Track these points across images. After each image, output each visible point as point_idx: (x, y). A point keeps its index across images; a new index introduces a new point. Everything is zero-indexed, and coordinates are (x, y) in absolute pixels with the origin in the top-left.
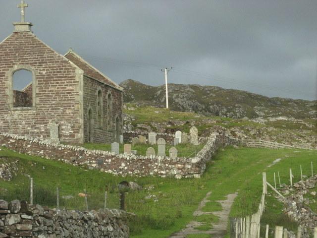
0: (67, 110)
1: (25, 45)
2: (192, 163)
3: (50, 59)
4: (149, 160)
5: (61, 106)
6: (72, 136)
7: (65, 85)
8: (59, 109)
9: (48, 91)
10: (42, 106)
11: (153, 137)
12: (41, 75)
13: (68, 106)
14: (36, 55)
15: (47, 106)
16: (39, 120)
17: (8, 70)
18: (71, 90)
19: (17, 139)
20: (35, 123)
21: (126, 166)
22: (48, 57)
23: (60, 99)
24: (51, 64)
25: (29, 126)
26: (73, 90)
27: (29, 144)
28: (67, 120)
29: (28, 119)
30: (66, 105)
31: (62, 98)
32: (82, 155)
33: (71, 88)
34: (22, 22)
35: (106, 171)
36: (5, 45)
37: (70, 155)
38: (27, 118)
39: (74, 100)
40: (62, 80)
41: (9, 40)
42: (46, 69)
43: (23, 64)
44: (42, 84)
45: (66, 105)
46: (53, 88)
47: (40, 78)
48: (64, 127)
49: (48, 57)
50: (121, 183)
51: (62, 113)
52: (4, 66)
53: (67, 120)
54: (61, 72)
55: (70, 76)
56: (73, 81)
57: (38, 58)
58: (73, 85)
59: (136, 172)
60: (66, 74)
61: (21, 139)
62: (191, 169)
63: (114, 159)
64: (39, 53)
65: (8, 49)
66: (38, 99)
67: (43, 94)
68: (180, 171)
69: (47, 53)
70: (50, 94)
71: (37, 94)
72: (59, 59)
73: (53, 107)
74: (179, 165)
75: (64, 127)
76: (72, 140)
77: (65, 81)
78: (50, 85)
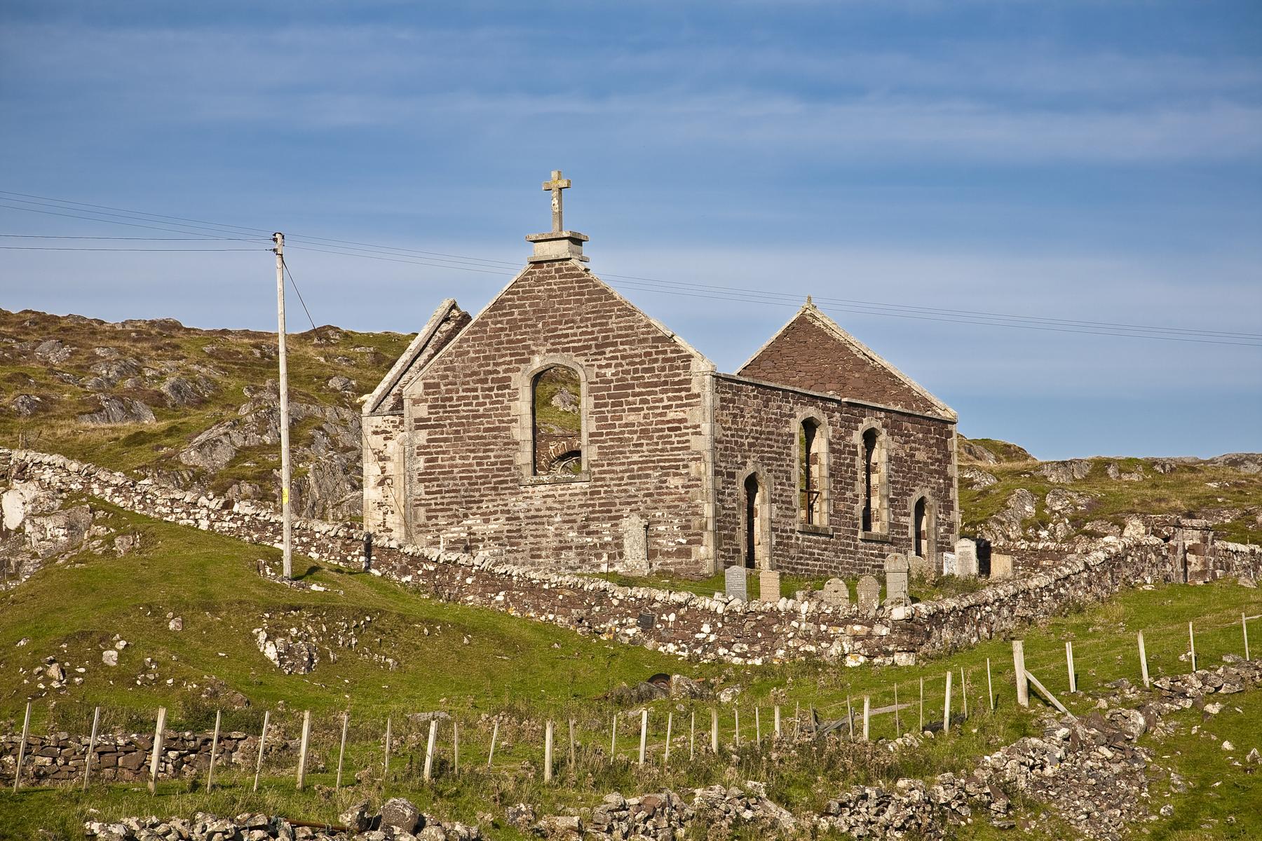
0: (669, 479)
1: (561, 296)
2: (893, 622)
3: (623, 332)
4: (774, 614)
5: (654, 468)
6: (684, 552)
7: (664, 407)
8: (648, 476)
9: (620, 426)
10: (606, 468)
11: (968, 553)
12: (601, 382)
13: (670, 467)
14: (589, 323)
15: (618, 468)
16: (597, 508)
17: (519, 370)
18: (680, 421)
19: (441, 561)
20: (586, 520)
21: (712, 632)
22: (620, 329)
23: (651, 447)
24: (626, 347)
25: (572, 528)
26: (685, 420)
27: (470, 575)
28: (669, 507)
29: (569, 508)
30: (667, 464)
31: (657, 444)
32: (601, 604)
33: (681, 415)
34: (554, 231)
35: (661, 649)
36: (509, 300)
37: (569, 603)
38: (567, 504)
39: (688, 448)
40: (656, 393)
41: (518, 287)
42: (613, 362)
43: (556, 351)
44: (605, 405)
45: (667, 464)
46: (632, 418)
47: (600, 389)
48: (661, 528)
49: (620, 329)
50: (651, 680)
51: (657, 488)
52: (508, 359)
53: (669, 507)
54: (652, 370)
55: (676, 379)
56: (683, 394)
57: (592, 333)
58: (685, 405)
59: (738, 650)
60: (666, 376)
61: (449, 562)
62: (889, 638)
63: (682, 611)
64: (595, 319)
65: (516, 311)
66: (594, 449)
67: (607, 434)
68: (858, 645)
69: (618, 317)
70: (626, 435)
71: (591, 435)
72: (648, 333)
73: (632, 470)
74: (857, 628)
75: (661, 528)
76: (683, 566)
77: (664, 396)
78: (626, 408)
